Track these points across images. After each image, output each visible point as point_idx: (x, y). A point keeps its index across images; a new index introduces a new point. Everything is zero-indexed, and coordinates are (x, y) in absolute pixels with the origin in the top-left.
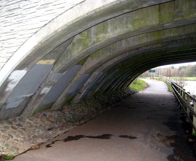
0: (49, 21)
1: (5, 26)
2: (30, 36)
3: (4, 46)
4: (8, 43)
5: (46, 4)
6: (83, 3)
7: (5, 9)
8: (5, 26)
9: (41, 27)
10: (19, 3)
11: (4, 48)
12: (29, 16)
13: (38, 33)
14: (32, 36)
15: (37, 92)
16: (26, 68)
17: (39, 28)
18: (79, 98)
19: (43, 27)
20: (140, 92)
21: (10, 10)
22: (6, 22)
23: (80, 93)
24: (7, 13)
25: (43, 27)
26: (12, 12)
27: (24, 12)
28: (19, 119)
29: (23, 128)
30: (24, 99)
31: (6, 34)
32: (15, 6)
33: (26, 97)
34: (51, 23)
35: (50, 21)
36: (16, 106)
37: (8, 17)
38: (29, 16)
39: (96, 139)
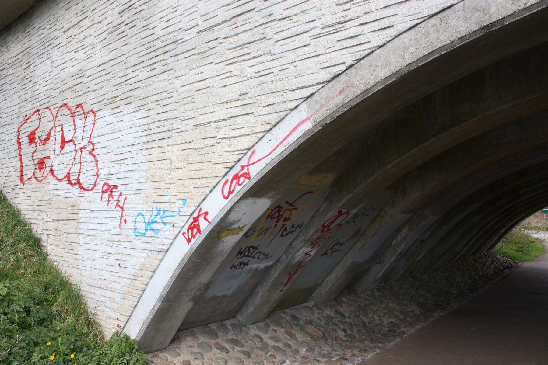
0: (348, 63)
1: (225, 86)
2: (293, 107)
3: (220, 135)
4: (232, 127)
5: (340, 23)
6: (447, 12)
7: (227, 44)
8: (225, 86)
9: (323, 83)
10: (264, 26)
11: (219, 141)
12: (291, 57)
13: (316, 97)
14: (296, 107)
15: (284, 256)
16: (273, 193)
17: (317, 84)
18: (378, 276)
19: (328, 82)
20: (526, 265)
21: (239, 46)
22: (226, 75)
23: (380, 263)
24: (231, 55)
25: (328, 82)
26: (245, 51)
27: (277, 48)
28: (233, 325)
29: (245, 349)
30: (250, 275)
31: (225, 106)
32: (253, 35)
33: (257, 269)
34: (353, 70)
35: (351, 66)
36: (228, 293)
37: (235, 63)
38: (291, 57)
39: (91, 305)
